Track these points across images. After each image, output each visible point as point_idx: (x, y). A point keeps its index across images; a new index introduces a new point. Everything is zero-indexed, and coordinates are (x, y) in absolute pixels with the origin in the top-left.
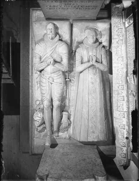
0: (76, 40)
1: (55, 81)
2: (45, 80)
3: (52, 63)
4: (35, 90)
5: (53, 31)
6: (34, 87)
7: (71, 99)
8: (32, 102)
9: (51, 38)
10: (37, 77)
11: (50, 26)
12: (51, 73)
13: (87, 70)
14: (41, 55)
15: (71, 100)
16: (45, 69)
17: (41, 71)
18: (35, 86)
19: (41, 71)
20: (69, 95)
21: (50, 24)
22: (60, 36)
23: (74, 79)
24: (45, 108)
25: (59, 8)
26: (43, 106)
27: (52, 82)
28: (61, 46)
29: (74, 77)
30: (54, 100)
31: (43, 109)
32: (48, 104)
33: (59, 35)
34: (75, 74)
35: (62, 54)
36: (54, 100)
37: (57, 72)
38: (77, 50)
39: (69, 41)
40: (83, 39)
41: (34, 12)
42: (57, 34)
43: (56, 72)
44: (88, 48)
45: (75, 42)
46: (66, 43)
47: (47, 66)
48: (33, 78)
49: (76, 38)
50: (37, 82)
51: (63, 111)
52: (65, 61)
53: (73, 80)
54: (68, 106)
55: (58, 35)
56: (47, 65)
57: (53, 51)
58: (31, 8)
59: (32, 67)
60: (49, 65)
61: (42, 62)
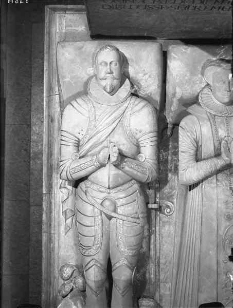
0: (178, 95)
1: (120, 210)
2: (90, 208)
3: (113, 159)
4: (59, 234)
5: (115, 68)
6: (56, 228)
7: (162, 261)
8: (49, 273)
9: (108, 90)
10: (65, 197)
11: (107, 55)
12: (109, 188)
13: (213, 179)
14: (80, 137)
15: (161, 266)
16: (90, 177)
17: (76, 183)
18: (59, 225)
19: (76, 183)
20: (158, 251)
21: (108, 49)
22: (132, 86)
23: (169, 204)
24: (91, 288)
25: (138, 7)
26: (85, 283)
27: (113, 214)
28: (138, 111)
29: (170, 198)
30: (118, 265)
31: (84, 291)
32: (99, 278)
33: (129, 79)
34: (172, 188)
35: (141, 134)
36: (118, 265)
37: (126, 186)
38: (182, 123)
39: (158, 98)
40: (199, 91)
41: (57, 16)
42: (124, 76)
43: (123, 184)
44: (215, 115)
45: (175, 100)
46: (148, 99)
47: (99, 168)
48: (53, 201)
49: (178, 90)
50: (65, 213)
51: (138, 299)
52: (148, 152)
53: (168, 207)
54: (153, 281)
55: (127, 79)
56: (97, 164)
57: (114, 125)
58: (48, 4)
59: (50, 168)
60: (102, 166)
61: (83, 157)
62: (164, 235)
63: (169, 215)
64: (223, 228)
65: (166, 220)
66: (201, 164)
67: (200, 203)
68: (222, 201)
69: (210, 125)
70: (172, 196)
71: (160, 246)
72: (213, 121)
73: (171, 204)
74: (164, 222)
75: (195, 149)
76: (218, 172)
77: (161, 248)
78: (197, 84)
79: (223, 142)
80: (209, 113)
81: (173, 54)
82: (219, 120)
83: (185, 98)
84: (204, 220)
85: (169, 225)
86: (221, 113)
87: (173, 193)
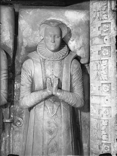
23: (20, 119)
44: (45, 60)
45: (23, 47)
49: (24, 41)
53: (19, 121)
62: (16, 140)
63: (20, 127)
64: (47, 141)
65: (18, 130)
66: (33, 94)
67: (33, 121)
68: (47, 121)
69: (40, 67)
70: (22, 113)
71: (13, 147)
72: (43, 64)
73: (21, 119)
74: (16, 131)
75: (30, 83)
76: (46, 99)
77: (14, 148)
78: (37, 36)
79: (48, 79)
80: (41, 57)
81: (20, 15)
82: (48, 63)
83: (30, 46)
84: (35, 133)
85: (20, 133)
86: (48, 58)
87: (22, 112)
